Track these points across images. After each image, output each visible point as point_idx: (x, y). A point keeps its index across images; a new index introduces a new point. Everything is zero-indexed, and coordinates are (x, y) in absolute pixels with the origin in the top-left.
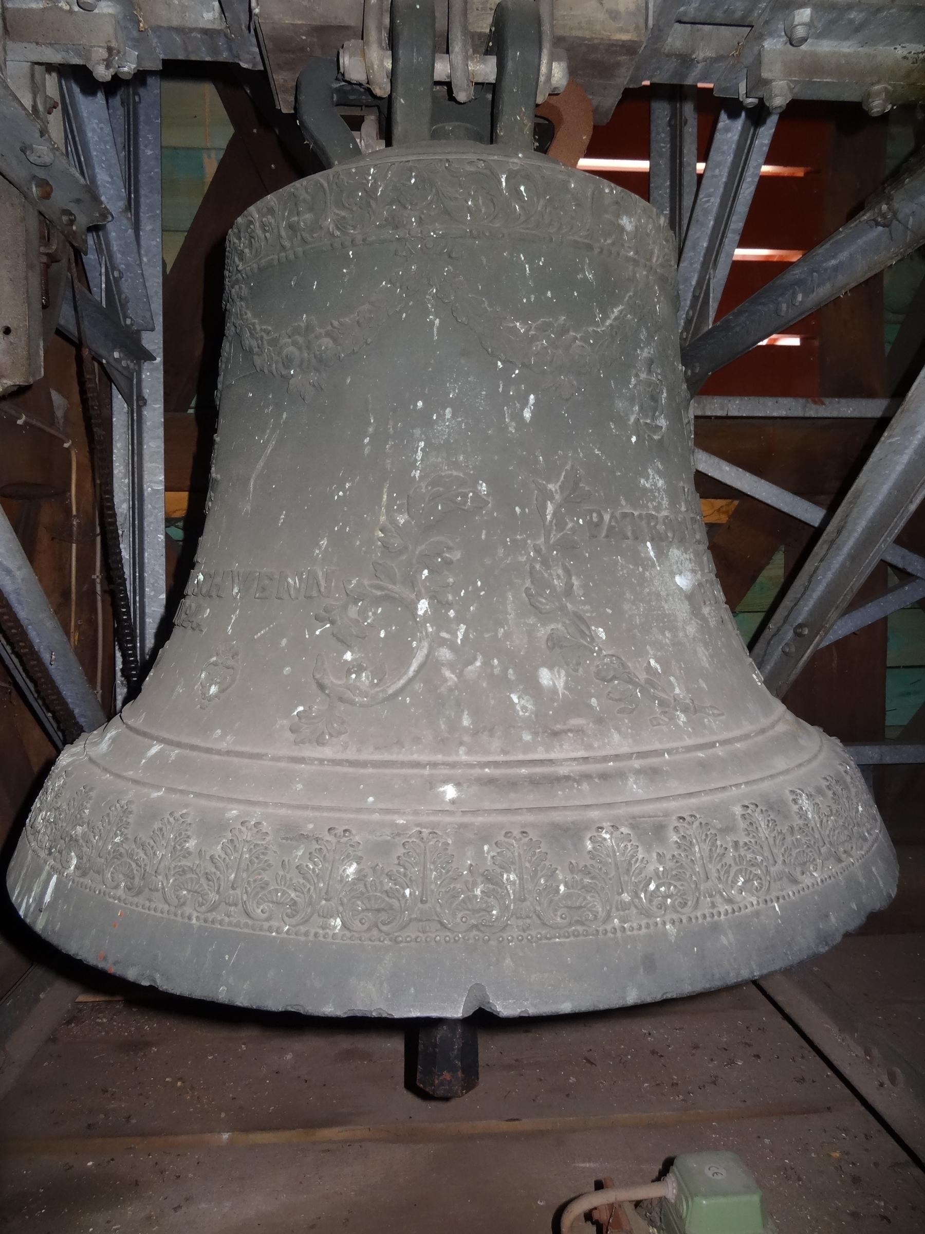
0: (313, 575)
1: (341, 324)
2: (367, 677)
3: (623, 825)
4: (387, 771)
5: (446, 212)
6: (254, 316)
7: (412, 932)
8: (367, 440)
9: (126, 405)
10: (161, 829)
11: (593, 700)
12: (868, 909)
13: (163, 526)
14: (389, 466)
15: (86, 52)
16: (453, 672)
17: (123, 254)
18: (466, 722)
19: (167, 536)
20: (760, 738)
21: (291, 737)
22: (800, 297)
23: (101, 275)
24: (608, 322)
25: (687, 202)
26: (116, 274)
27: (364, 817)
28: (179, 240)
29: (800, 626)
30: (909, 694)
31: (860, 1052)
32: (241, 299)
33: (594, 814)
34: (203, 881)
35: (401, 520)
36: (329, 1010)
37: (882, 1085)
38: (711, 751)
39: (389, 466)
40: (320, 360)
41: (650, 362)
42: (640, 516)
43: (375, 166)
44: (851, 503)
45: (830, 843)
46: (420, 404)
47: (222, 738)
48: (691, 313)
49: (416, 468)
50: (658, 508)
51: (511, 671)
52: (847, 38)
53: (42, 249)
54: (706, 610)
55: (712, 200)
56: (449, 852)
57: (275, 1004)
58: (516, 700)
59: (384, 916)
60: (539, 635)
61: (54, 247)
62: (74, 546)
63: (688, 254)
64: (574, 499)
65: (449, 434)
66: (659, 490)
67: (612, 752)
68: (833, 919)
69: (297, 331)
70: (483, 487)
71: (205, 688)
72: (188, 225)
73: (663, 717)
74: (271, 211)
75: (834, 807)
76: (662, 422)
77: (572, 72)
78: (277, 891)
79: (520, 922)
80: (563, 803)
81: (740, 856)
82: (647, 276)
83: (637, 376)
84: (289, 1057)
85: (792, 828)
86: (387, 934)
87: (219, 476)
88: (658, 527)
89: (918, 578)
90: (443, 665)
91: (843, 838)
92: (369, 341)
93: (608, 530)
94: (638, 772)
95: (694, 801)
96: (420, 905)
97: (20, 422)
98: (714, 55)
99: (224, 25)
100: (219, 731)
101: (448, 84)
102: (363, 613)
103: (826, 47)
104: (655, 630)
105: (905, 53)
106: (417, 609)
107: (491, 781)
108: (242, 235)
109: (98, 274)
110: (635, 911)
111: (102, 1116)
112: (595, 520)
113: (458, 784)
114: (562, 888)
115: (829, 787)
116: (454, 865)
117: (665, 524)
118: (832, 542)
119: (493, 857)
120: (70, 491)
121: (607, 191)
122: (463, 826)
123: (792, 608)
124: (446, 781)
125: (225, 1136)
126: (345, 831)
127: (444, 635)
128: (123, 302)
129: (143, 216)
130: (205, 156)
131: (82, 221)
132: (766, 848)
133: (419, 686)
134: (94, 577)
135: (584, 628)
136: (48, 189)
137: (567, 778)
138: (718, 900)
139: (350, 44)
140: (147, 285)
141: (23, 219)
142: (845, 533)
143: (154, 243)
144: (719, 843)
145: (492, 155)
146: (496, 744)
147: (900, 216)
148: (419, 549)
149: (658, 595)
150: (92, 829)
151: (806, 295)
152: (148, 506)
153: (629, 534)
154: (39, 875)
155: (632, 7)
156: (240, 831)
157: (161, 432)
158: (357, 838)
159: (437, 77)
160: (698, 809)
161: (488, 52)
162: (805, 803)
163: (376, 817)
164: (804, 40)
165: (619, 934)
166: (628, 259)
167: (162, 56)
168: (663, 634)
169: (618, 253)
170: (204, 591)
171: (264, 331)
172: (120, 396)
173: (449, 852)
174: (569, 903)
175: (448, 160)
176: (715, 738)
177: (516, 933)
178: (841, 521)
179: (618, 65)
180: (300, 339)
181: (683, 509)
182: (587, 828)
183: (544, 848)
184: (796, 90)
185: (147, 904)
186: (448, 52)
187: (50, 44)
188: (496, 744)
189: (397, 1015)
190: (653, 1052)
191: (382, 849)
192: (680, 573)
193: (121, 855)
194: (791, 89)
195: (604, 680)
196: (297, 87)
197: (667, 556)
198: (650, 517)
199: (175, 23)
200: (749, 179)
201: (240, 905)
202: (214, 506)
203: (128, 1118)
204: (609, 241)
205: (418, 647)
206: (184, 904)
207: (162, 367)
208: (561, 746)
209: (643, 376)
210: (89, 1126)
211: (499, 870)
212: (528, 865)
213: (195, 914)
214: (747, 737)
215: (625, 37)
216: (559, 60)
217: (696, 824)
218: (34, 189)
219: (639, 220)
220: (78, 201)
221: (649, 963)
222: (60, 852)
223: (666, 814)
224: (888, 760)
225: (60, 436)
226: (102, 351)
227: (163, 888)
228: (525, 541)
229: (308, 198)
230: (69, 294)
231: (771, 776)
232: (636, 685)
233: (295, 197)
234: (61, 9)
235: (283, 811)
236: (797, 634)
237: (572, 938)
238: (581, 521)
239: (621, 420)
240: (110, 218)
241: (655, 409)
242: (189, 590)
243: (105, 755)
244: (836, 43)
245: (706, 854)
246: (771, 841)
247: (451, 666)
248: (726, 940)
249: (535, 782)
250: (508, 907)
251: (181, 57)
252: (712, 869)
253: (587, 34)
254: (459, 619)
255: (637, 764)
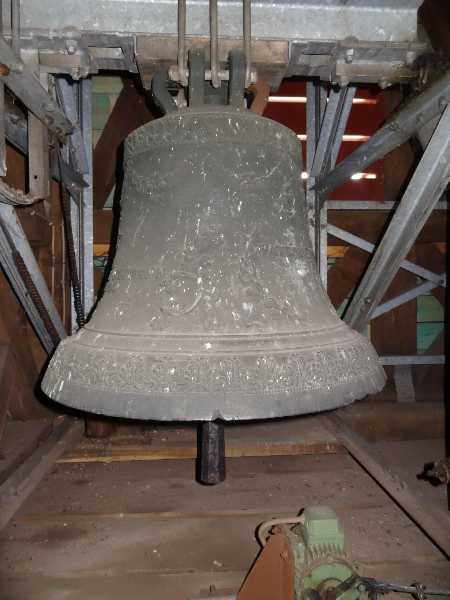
0: (159, 270)
1: (169, 175)
2: (179, 306)
3: (271, 357)
4: (186, 339)
5: (208, 133)
6: (136, 172)
7: (194, 392)
8: (179, 219)
9: (76, 207)
10: (103, 361)
11: (263, 315)
12: (367, 393)
13: (92, 259)
14: (187, 229)
15: (70, 69)
16: (210, 304)
17: (76, 141)
18: (215, 322)
19: (94, 265)
20: (330, 331)
21: (150, 328)
22: (365, 158)
23: (67, 151)
24: (271, 174)
25: (322, 116)
26: (73, 150)
27: (177, 354)
28: (99, 134)
29: (367, 298)
30: (429, 334)
31: (390, 477)
32: (131, 165)
33: (261, 353)
34: (119, 377)
35: (192, 248)
36: (165, 418)
37: (398, 489)
38: (308, 334)
39: (187, 229)
40: (161, 189)
41: (288, 189)
42: (283, 247)
43: (181, 116)
44: (383, 245)
45: (352, 368)
46: (199, 205)
47: (125, 330)
48: (324, 164)
49: (197, 229)
50: (291, 244)
51: (232, 304)
52: (370, 59)
53: (49, 144)
54: (311, 284)
55: (331, 116)
56: (208, 365)
57: (146, 417)
58: (234, 314)
59: (184, 387)
60: (243, 291)
61: (53, 143)
62: (53, 268)
63: (322, 139)
64: (257, 240)
65: (210, 216)
66: (291, 237)
67: (270, 333)
68: (351, 394)
69: (152, 178)
70: (222, 236)
71: (118, 313)
72: (103, 127)
73: (290, 321)
74: (142, 132)
75: (356, 356)
76: (293, 211)
77: (259, 75)
78: (146, 379)
79: (232, 389)
80: (250, 350)
81: (315, 369)
82: (287, 156)
83: (282, 194)
84: (148, 487)
85: (336, 361)
86: (185, 393)
87: (122, 234)
88: (291, 251)
89: (429, 281)
90: (207, 301)
91: (358, 367)
92: (180, 181)
93: (270, 252)
94: (278, 340)
95: (299, 350)
96: (197, 383)
97: (32, 214)
98: (318, 65)
99: (123, 57)
100: (124, 328)
101: (211, 81)
102: (177, 283)
103: (362, 63)
104: (288, 290)
105: (394, 65)
106: (197, 281)
107: (224, 342)
108: (131, 141)
109: (65, 150)
110: (274, 386)
111: (69, 508)
112: (265, 248)
113: (211, 343)
114: (248, 377)
115: (354, 349)
116: (209, 369)
117: (293, 250)
118: (377, 262)
119: (223, 367)
120: (51, 244)
121: (270, 124)
122: (214, 357)
123: (363, 291)
124: (207, 342)
125: (122, 515)
126: (170, 358)
127: (207, 291)
128: (76, 162)
129: (84, 125)
130: (110, 96)
131: (64, 131)
132: (325, 367)
133: (198, 309)
134: (62, 282)
135: (260, 288)
136: (52, 120)
137: (252, 341)
138: (306, 384)
139: (172, 67)
140: (86, 154)
141: (43, 133)
142: (382, 258)
143: (89, 136)
144: (307, 364)
145: (226, 111)
146: (226, 330)
147: (400, 127)
148: (198, 259)
149: (290, 277)
150: (77, 363)
151: (368, 157)
152: (86, 250)
153: (279, 254)
154: (56, 382)
155: (282, 50)
156: (133, 359)
157: (91, 218)
158: (175, 361)
159: (206, 79)
160: (301, 353)
161: (226, 69)
162: (343, 353)
163: (182, 354)
164: (351, 61)
165: (268, 393)
166: (278, 149)
167: (98, 68)
168: (292, 291)
169: (275, 148)
170: (117, 277)
171: (140, 178)
172: (74, 203)
173: (208, 365)
174: (250, 383)
175: (209, 114)
176: (310, 330)
177: (231, 392)
178: (380, 252)
179: (278, 72)
180: (153, 181)
181: (302, 245)
182: (258, 357)
183: (242, 363)
184: (351, 79)
185: (99, 386)
186: (210, 69)
187: (56, 67)
188: (226, 330)
189: (189, 419)
190: (307, 485)
191: (184, 364)
192: (300, 269)
193: (89, 371)
194: (348, 79)
195: (267, 307)
196: (152, 81)
197: (294, 262)
198: (287, 248)
199: (104, 56)
200: (347, 107)
201: (133, 385)
202: (120, 246)
203: (80, 508)
204: (271, 143)
205: (198, 295)
206: (112, 385)
207: (92, 190)
208: (250, 330)
209: (285, 194)
210: (64, 511)
211: (225, 371)
212: (236, 369)
213: (116, 389)
214: (324, 330)
215: (280, 62)
216: (253, 72)
217: (299, 357)
218: (47, 120)
219: (283, 134)
220: (63, 124)
221: (279, 404)
222: (64, 373)
223: (288, 354)
224: (416, 363)
225: (48, 220)
226: (68, 184)
227: (105, 381)
228: (238, 256)
229: (156, 128)
230: (57, 160)
231: (331, 344)
232: (280, 310)
233: (152, 127)
234: (60, 53)
235: (148, 353)
236: (366, 302)
237: (251, 394)
238: (260, 249)
239: (276, 211)
240: (75, 130)
241: (290, 207)
242: (110, 278)
243: (79, 340)
244: (366, 61)
245: (302, 367)
246: (328, 365)
247: (210, 302)
248: (308, 397)
249: (240, 343)
250: (228, 384)
251: (106, 69)
252: (304, 373)
253: (265, 61)
254: (213, 285)
255: (278, 337)
